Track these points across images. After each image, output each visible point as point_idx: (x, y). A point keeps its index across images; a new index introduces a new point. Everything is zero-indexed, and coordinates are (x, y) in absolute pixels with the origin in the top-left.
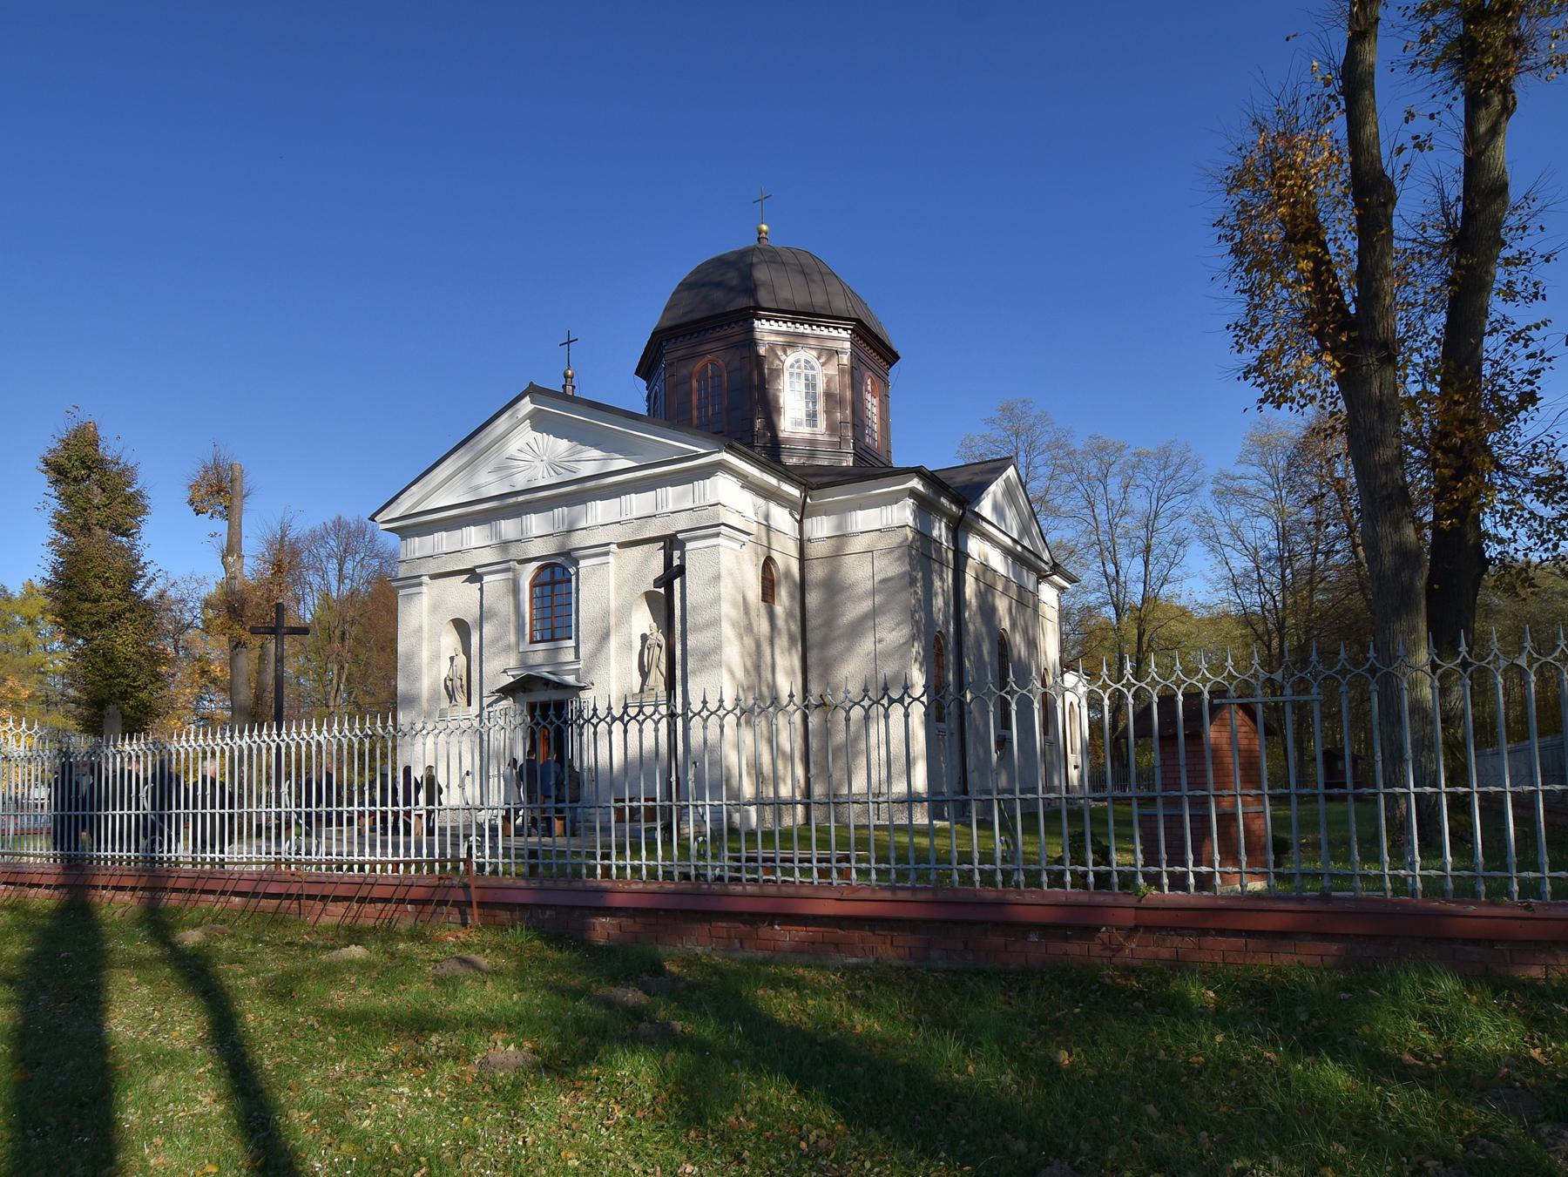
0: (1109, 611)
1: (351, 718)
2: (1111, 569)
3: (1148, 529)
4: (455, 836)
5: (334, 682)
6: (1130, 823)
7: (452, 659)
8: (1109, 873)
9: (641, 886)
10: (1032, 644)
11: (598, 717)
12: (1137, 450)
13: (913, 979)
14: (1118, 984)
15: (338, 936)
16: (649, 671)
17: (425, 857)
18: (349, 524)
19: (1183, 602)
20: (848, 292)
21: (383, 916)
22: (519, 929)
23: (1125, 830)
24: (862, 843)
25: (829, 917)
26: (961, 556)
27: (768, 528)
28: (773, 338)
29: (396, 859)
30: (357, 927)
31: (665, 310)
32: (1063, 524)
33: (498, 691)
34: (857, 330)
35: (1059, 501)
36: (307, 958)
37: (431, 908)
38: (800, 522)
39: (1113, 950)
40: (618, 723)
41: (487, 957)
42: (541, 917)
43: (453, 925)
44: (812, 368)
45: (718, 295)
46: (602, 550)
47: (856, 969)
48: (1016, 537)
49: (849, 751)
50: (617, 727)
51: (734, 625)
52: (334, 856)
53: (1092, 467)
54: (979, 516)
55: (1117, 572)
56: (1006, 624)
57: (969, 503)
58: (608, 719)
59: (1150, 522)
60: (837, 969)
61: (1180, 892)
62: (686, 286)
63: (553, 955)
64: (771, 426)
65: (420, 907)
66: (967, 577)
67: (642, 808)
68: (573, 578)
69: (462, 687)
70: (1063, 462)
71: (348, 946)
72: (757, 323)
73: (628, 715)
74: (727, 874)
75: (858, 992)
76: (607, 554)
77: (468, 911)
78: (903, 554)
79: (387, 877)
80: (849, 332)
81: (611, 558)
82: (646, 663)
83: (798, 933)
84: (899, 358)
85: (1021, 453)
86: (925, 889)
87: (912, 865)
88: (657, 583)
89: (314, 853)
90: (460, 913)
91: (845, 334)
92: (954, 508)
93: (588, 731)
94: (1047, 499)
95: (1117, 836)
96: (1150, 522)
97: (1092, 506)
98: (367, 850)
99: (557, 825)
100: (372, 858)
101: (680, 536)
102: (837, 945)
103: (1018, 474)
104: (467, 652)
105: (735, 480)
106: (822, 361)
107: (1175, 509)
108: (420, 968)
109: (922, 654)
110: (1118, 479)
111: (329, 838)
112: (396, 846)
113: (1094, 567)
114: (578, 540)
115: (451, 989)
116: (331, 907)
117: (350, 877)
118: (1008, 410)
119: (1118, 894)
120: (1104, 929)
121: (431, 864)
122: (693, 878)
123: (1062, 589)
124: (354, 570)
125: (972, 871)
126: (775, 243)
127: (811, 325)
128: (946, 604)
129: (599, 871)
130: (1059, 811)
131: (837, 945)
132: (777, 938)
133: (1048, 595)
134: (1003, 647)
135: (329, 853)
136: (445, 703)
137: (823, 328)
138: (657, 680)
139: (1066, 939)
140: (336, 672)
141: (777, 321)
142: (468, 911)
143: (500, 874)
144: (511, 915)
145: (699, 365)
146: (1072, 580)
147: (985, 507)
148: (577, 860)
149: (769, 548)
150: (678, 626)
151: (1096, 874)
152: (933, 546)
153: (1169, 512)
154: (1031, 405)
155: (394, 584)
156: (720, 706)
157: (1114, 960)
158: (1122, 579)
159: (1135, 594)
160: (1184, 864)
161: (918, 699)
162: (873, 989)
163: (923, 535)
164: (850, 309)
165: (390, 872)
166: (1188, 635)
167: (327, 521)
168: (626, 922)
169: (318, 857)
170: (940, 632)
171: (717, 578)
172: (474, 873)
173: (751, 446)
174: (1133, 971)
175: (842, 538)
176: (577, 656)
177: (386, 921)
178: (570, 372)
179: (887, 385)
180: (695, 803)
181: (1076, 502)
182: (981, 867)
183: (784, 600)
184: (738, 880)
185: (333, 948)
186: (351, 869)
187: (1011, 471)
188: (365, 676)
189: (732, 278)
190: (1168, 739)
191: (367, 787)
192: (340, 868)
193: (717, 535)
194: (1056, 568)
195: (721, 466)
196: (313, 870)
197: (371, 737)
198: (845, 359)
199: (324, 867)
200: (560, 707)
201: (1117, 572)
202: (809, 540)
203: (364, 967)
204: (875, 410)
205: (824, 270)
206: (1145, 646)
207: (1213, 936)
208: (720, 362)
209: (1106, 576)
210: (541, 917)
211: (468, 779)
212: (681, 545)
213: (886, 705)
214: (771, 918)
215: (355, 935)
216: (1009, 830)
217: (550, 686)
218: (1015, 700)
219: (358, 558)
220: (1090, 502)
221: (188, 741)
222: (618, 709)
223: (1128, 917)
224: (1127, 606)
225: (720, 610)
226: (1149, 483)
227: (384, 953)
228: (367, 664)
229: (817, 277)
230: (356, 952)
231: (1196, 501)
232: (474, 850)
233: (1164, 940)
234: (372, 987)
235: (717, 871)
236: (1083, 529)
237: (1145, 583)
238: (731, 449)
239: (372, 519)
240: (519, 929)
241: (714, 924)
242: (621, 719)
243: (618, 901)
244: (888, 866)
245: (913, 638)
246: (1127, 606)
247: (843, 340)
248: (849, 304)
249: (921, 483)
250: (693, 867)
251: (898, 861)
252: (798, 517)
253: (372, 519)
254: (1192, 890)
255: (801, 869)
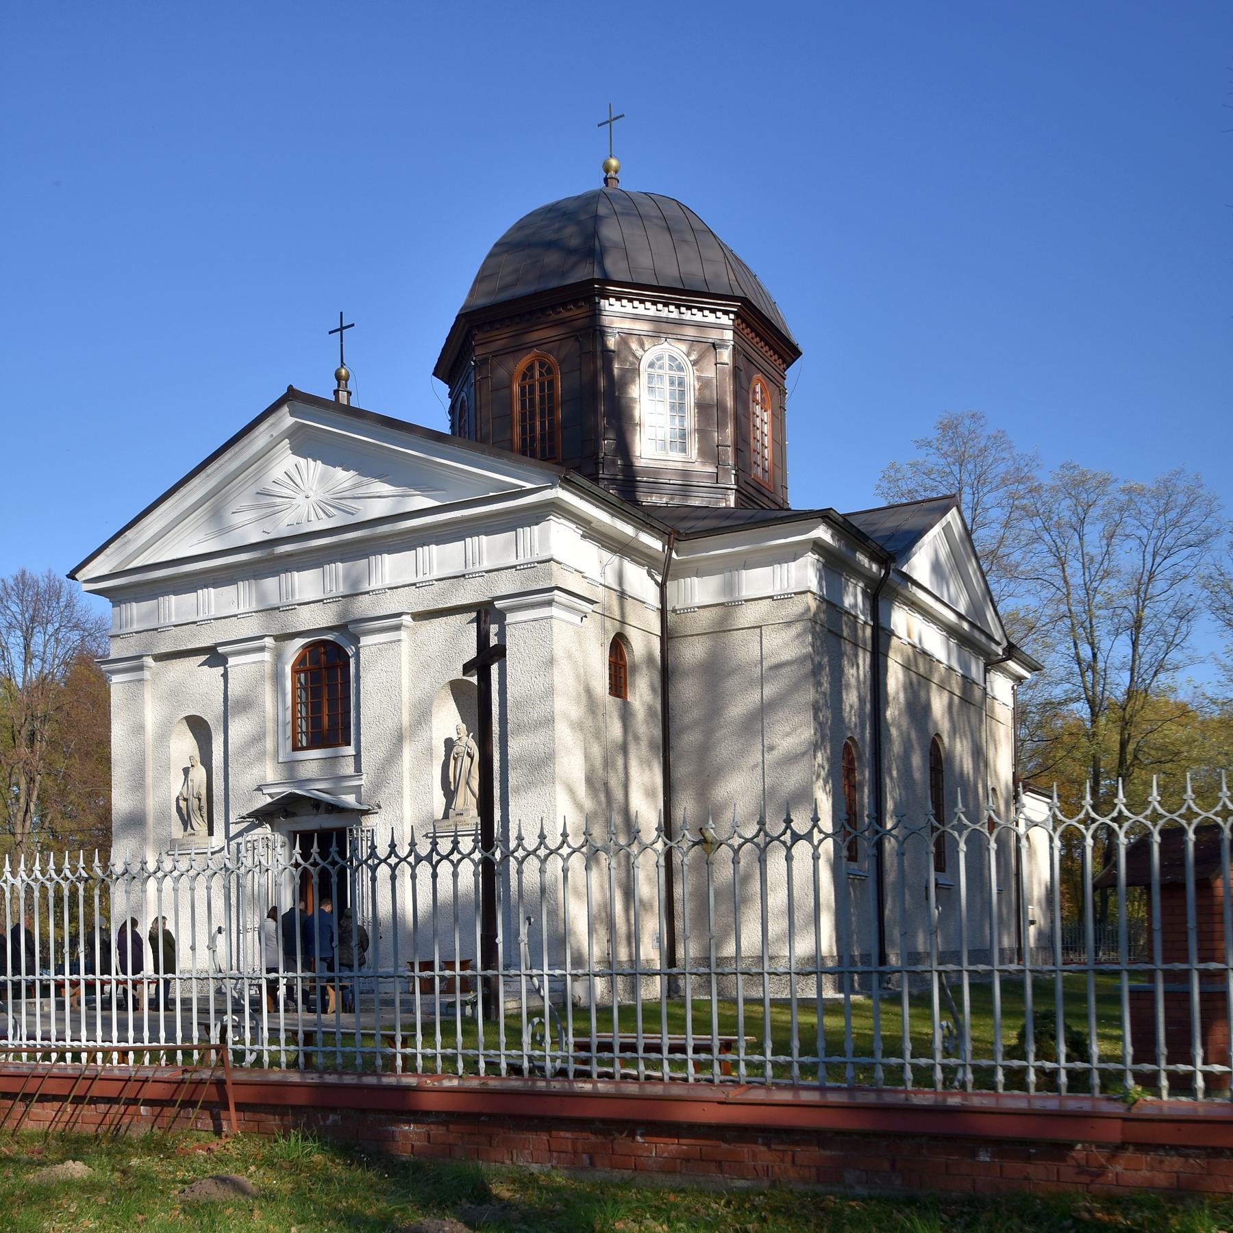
0: (1082, 710)
1: (45, 848)
2: (1085, 651)
3: (1139, 596)
4: (204, 1011)
5: (22, 800)
6: (1117, 1000)
7: (186, 771)
8: (1088, 1072)
9: (455, 1083)
10: (979, 755)
11: (397, 856)
12: (1127, 485)
13: (823, 1209)
14: (1099, 1220)
15: (47, 1148)
16: (457, 788)
17: (162, 1043)
18: (37, 581)
19: (1183, 696)
20: (730, 258)
21: (107, 1120)
22: (293, 1140)
23: (1110, 1010)
24: (754, 1025)
25: (709, 1127)
26: (881, 633)
27: (622, 595)
28: (627, 325)
29: (123, 1044)
30: (73, 1136)
31: (476, 282)
32: (1022, 589)
33: (250, 816)
34: (743, 314)
35: (1016, 556)
36: (7, 1178)
37: (170, 1112)
38: (662, 587)
39: (1090, 1174)
40: (445, 863)
41: (251, 1176)
42: (322, 1123)
43: (203, 1134)
44: (680, 369)
45: (553, 259)
46: (391, 622)
47: (745, 1194)
48: (963, 612)
49: (735, 899)
50: (424, 870)
51: (578, 726)
52: (39, 1041)
53: (1064, 509)
54: (908, 578)
55: (1094, 655)
56: (944, 725)
57: (894, 560)
58: (411, 859)
59: (1141, 588)
60: (720, 1196)
61: (1183, 1099)
62: (505, 247)
63: (338, 1169)
64: (624, 449)
65: (158, 1109)
66: (890, 663)
67: (458, 979)
68: (352, 661)
69: (200, 809)
70: (1025, 501)
71: (62, 1161)
72: (604, 303)
73: (438, 854)
74: (572, 1067)
75: (750, 1227)
76: (397, 628)
77: (223, 1114)
78: (805, 632)
79: (111, 1069)
80: (732, 316)
81: (403, 634)
82: (452, 780)
83: (669, 1147)
84: (800, 354)
85: (967, 490)
86: (839, 1089)
87: (822, 1057)
88: (467, 668)
89: (10, 1037)
90: (212, 1117)
91: (725, 320)
92: (875, 567)
93: (366, 873)
94: (1000, 552)
95: (1099, 1018)
96: (1141, 588)
97: (1063, 565)
98: (84, 1033)
99: (333, 997)
100: (91, 1044)
101: (499, 604)
102: (719, 1163)
103: (963, 520)
104: (207, 761)
105: (574, 526)
106: (693, 357)
107: (1178, 568)
108: (162, 1192)
109: (827, 767)
110: (1100, 526)
111: (31, 1014)
112: (123, 1026)
113: (1061, 648)
114: (364, 606)
115: (206, 1220)
116: (36, 1109)
117: (59, 1068)
118: (949, 428)
119: (1098, 1099)
120: (1079, 1147)
121: (187, 1053)
122: (526, 1073)
123: (1019, 679)
124: (45, 646)
125: (932, 1067)
126: (629, 184)
127: (678, 307)
128: (861, 700)
129: (399, 1062)
130: (1021, 985)
131: (719, 1163)
132: (639, 1152)
133: (1001, 687)
134: (937, 761)
135: (31, 1037)
136: (177, 831)
137: (695, 311)
138: (468, 801)
139: (1028, 1158)
140: (23, 786)
141: (631, 300)
142: (223, 1114)
143: (266, 1066)
144: (282, 1120)
145: (523, 363)
146: (1034, 667)
147: (920, 565)
148: (369, 1046)
149: (623, 622)
150: (496, 728)
151: (1070, 1072)
152: (845, 618)
153: (1168, 573)
154: (982, 422)
155: (104, 667)
156: (563, 842)
157: (1092, 1187)
158: (1101, 665)
159: (1119, 684)
160: (1191, 1062)
161: (778, 838)
162: (769, 1221)
163: (831, 605)
164: (734, 283)
165: (115, 1062)
166: (1190, 742)
167: (5, 576)
168: (437, 1131)
169: (17, 1042)
170: (851, 738)
171: (551, 662)
172: (231, 1065)
173: (595, 479)
174: (1119, 1203)
175: (728, 607)
176: (358, 769)
177: (113, 1127)
178: (343, 371)
179: (783, 392)
180: (529, 972)
181: (1041, 558)
182: (915, 1061)
183: (642, 694)
184: (610, 1076)
185: (42, 1164)
186: (62, 1058)
187: (952, 516)
188: (63, 793)
189: (571, 235)
190: (1173, 888)
191: (67, 948)
192: (46, 1057)
193: (550, 603)
194: (1012, 651)
195: (555, 508)
196: (10, 1058)
197: (86, 880)
198: (726, 356)
199: (24, 1055)
200: (341, 834)
201: (1094, 655)
202: (674, 611)
203: (89, 1188)
204: (766, 429)
205: (696, 225)
206: (1129, 758)
207: (1228, 1158)
208: (552, 358)
209: (1079, 661)
210: (322, 1123)
211: (221, 939)
212: (500, 616)
213: (789, 844)
214: (630, 1126)
215: (74, 1147)
216: (952, 1013)
217: (322, 809)
218: (964, 838)
219: (50, 629)
220: (1059, 558)
221: (59, 871)
222: (576, 835)
223: (1114, 1133)
224: (1105, 704)
225: (552, 706)
226: (1143, 533)
227: (113, 1170)
228: (66, 776)
229: (689, 237)
230: (76, 1169)
231: (1207, 558)
232: (230, 1034)
233: (1161, 1162)
234: (100, 1217)
235: (558, 1064)
236: (1049, 595)
237: (1132, 670)
238: (568, 484)
239: (72, 576)
240: (293, 1140)
241: (554, 1133)
242: (429, 858)
243: (429, 1102)
244: (788, 1059)
245: (816, 746)
246: (1105, 704)
247: (722, 327)
248: (732, 277)
249: (830, 532)
250: (526, 1059)
251: (829, 1053)
252: (659, 579)
253: (72, 576)
254: (1200, 1096)
255: (671, 1062)
